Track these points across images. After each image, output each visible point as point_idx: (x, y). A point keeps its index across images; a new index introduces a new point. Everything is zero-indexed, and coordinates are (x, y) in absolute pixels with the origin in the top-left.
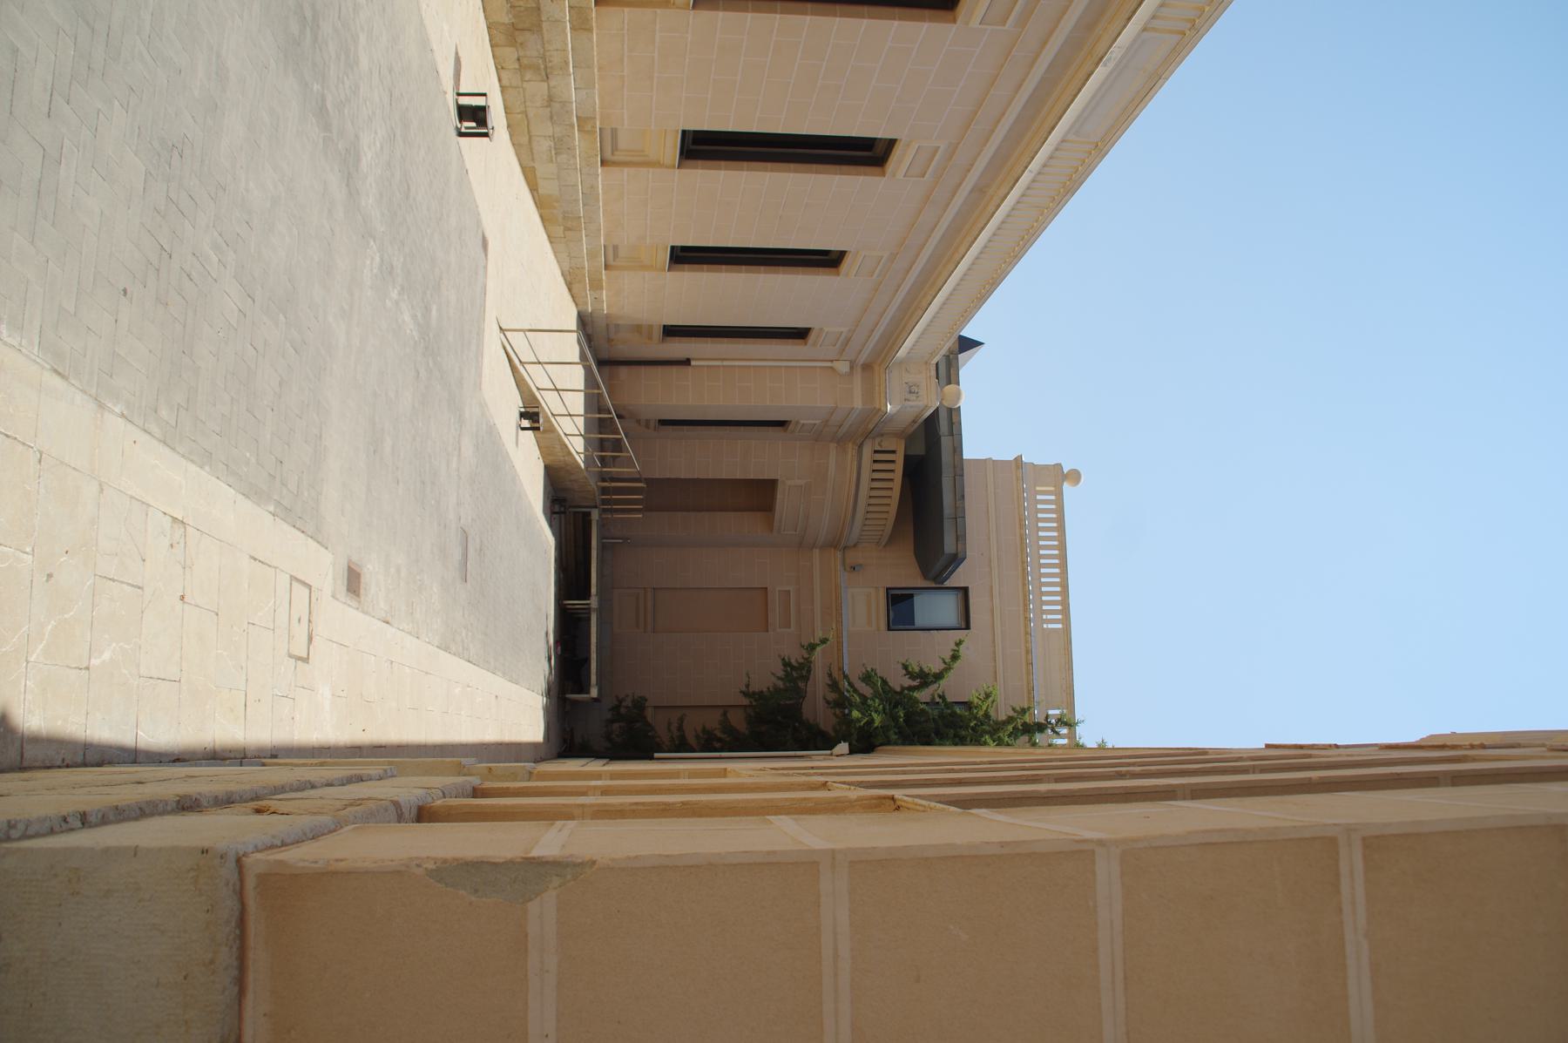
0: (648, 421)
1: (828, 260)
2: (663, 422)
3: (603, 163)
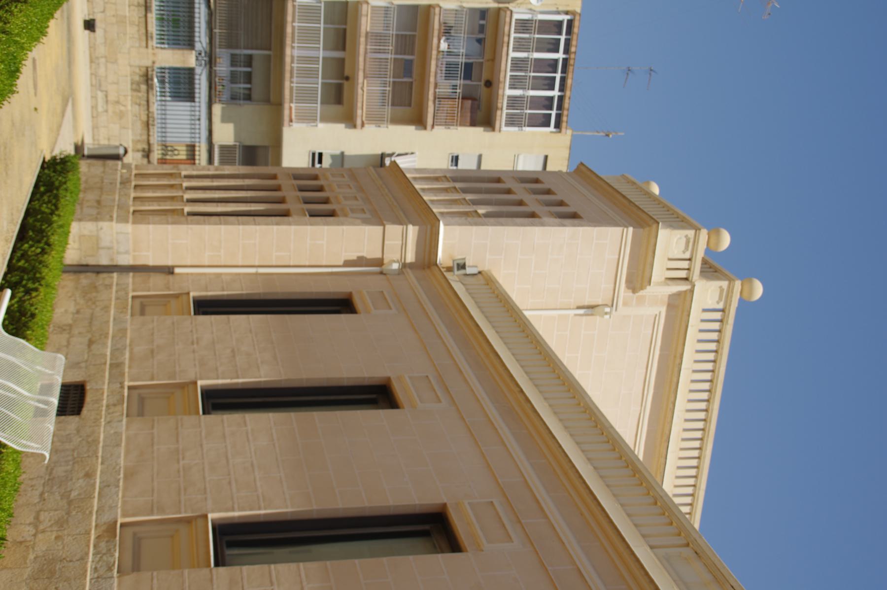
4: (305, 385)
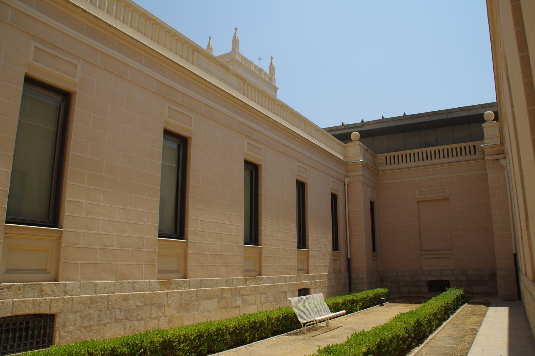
2: (336, 247)
4: (306, 212)
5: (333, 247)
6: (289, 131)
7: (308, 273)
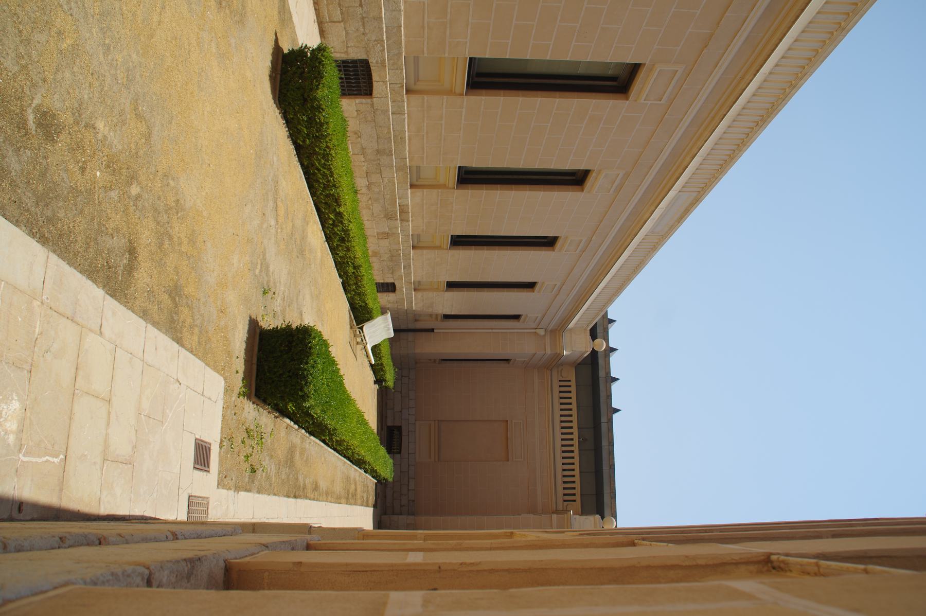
0: (437, 315)
1: (549, 242)
2: (447, 317)
3: (412, 186)
5: (458, 236)
6: (622, 248)
7: (412, 186)
